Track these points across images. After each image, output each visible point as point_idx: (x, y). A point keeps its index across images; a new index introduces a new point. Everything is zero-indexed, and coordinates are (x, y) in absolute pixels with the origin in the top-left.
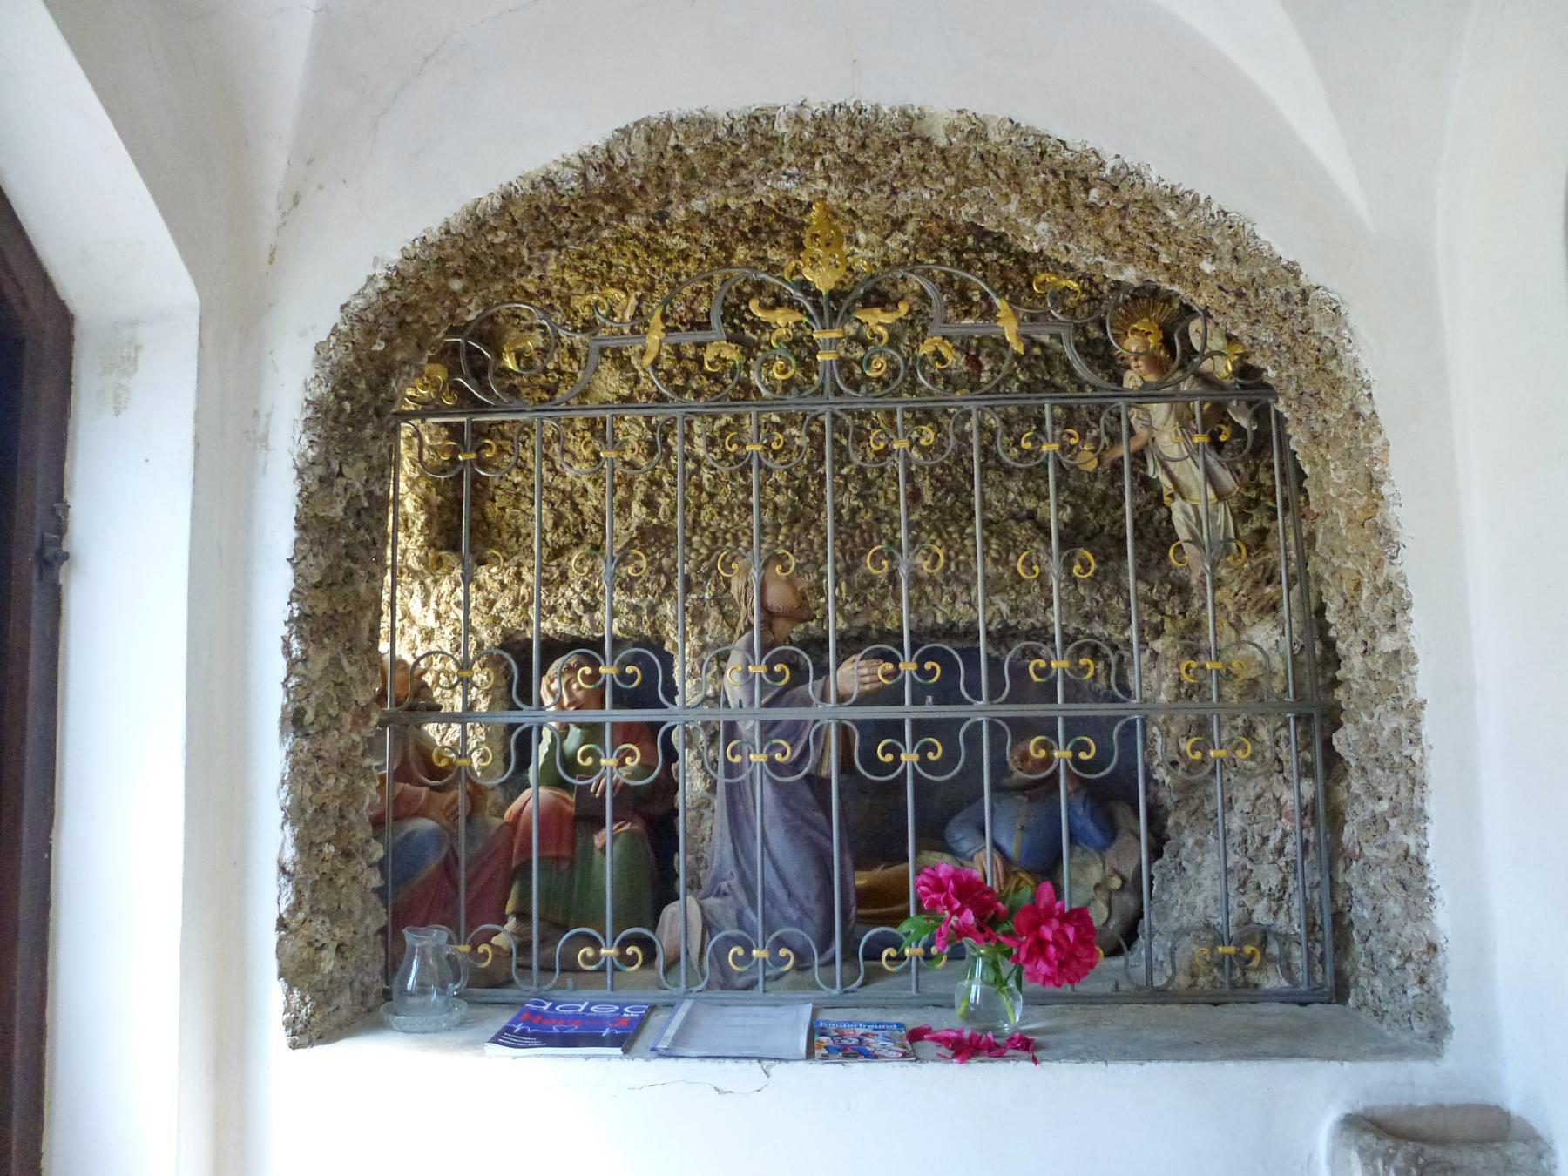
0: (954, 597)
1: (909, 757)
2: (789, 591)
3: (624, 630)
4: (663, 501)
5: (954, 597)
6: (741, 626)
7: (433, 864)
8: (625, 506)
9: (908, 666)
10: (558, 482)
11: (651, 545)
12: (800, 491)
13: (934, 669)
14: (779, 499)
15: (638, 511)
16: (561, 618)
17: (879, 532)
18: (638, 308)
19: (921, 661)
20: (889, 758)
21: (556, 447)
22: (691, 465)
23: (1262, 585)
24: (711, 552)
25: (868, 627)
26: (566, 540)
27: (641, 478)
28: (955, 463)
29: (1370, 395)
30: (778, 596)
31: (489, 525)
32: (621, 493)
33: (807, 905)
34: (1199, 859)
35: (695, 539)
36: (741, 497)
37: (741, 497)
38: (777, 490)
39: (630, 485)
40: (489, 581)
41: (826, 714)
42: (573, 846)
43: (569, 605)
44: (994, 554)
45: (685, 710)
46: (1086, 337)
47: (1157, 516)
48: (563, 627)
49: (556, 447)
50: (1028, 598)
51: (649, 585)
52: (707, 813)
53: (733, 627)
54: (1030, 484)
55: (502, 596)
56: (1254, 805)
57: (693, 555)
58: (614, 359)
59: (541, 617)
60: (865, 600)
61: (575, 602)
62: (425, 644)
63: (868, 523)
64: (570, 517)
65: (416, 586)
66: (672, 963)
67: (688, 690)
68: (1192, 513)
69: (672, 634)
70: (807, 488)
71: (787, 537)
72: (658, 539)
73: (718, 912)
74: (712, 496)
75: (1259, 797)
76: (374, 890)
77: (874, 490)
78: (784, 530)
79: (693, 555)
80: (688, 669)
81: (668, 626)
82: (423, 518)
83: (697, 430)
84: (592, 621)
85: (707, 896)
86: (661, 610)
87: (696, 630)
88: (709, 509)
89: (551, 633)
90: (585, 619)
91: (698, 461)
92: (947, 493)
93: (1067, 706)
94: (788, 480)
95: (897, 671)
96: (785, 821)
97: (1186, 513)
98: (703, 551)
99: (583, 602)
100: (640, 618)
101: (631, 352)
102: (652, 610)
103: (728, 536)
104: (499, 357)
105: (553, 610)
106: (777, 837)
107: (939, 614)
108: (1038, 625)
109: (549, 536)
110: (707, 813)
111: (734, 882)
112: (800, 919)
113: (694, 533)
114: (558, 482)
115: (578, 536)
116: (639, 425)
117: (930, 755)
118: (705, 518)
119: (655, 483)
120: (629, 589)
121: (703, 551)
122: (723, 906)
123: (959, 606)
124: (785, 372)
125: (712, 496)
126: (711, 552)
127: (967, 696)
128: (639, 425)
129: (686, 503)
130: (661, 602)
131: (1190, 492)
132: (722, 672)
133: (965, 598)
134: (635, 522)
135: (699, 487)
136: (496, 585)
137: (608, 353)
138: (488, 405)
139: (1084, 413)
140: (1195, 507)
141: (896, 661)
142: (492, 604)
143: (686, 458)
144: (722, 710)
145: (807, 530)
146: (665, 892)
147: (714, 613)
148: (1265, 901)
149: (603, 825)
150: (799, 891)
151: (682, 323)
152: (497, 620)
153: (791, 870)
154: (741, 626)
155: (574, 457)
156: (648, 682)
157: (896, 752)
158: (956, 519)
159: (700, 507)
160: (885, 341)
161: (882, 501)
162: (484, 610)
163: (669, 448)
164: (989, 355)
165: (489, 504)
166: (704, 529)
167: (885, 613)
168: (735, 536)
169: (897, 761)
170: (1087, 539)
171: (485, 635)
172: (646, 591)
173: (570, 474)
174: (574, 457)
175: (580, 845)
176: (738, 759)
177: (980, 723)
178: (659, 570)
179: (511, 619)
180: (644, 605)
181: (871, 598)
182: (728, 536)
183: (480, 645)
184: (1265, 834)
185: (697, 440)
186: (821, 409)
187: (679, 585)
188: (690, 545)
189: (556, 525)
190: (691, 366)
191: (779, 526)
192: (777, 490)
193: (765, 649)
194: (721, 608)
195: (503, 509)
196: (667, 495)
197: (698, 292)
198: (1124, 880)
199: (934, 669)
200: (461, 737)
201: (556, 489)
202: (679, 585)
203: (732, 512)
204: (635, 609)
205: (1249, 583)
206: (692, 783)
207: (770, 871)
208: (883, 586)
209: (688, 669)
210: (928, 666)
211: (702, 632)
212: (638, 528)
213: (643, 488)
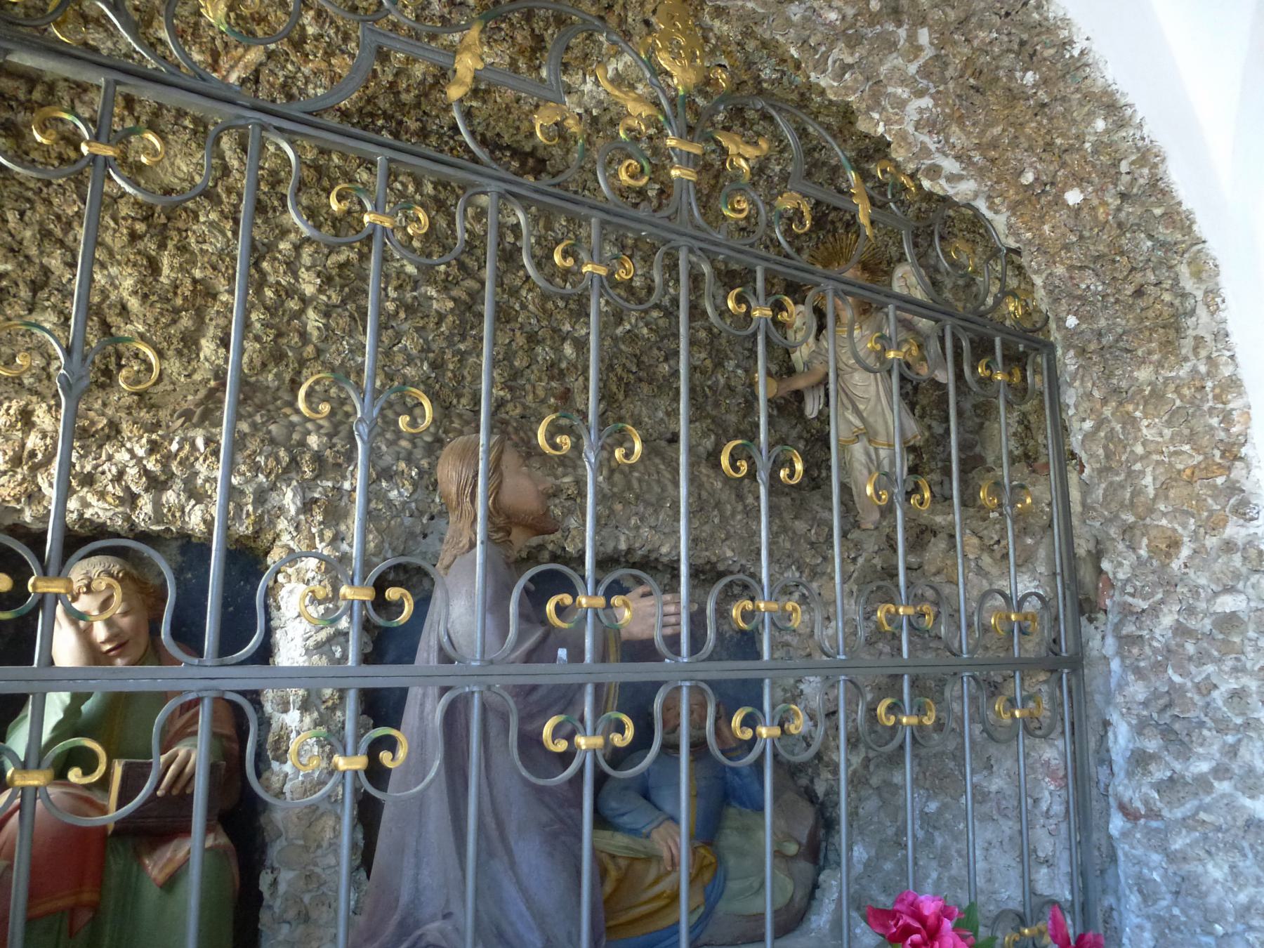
16: (102, 495)
18: (257, 72)
29: (1232, 357)
32: (186, 321)
43: (121, 474)
51: (261, 459)
58: (195, 132)
59: (66, 492)
68: (874, 457)
81: (282, 524)
83: (306, 260)
84: (157, 505)
86: (274, 498)
87: (328, 534)
93: (600, 667)
99: (146, 472)
100: (239, 507)
102: (261, 497)
105: (88, 480)
107: (623, 538)
116: (223, 233)
124: (632, 177)
128: (223, 233)
130: (273, 487)
135: (304, 335)
139: (724, 341)
149: (186, 831)
155: (111, 254)
161: (530, 397)
172: (257, 468)
174: (111, 254)
177: (473, 693)
180: (249, 490)
185: (303, 273)
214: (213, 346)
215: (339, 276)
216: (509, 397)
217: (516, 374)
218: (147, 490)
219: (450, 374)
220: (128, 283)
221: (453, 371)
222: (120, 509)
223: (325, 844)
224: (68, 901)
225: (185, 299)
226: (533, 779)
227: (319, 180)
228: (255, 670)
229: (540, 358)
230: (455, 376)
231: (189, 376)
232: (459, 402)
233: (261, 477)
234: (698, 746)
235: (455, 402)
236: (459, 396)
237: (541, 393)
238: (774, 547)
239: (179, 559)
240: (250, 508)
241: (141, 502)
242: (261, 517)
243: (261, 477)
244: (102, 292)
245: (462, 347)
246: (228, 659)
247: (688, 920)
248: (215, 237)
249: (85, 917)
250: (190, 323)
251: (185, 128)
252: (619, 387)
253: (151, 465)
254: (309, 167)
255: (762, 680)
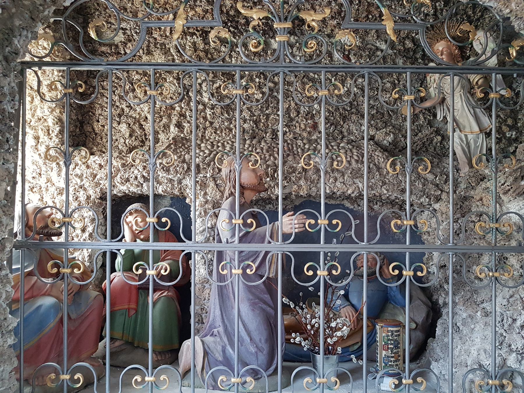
0: (336, 180)
1: (322, 273)
2: (253, 175)
3: (165, 191)
4: (186, 125)
5: (336, 180)
6: (227, 193)
7: (52, 323)
8: (166, 127)
9: (323, 222)
10: (132, 113)
11: (180, 147)
12: (256, 122)
13: (337, 223)
14: (246, 126)
15: (173, 130)
17: (296, 144)
19: (330, 219)
20: (311, 273)
21: (131, 94)
22: (201, 107)
23: (519, 180)
24: (211, 152)
25: (290, 194)
26: (136, 143)
27: (175, 113)
28: (335, 110)
30: (248, 178)
31: (96, 134)
32: (165, 120)
33: (260, 345)
34: (473, 326)
35: (203, 145)
36: (226, 124)
37: (226, 124)
38: (245, 121)
39: (169, 116)
40: (93, 164)
41: (278, 248)
42: (137, 303)
43: (136, 178)
44: (356, 158)
45: (197, 245)
46: (404, 47)
47: (435, 140)
48: (133, 189)
49: (131, 94)
50: (373, 181)
52: (207, 286)
53: (222, 192)
54: (372, 122)
55: (93, 173)
56: (508, 301)
57: (201, 154)
58: (161, 49)
60: (290, 179)
61: (139, 176)
62: (59, 196)
63: (291, 140)
64: (138, 132)
65: (54, 165)
66: (187, 372)
67: (198, 225)
68: (464, 139)
69: (190, 193)
70: (260, 121)
71: (250, 146)
72: (183, 145)
73: (212, 346)
74: (211, 123)
75: (511, 297)
76: (10, 346)
77: (294, 123)
78: (248, 142)
79: (201, 154)
80: (197, 213)
81: (188, 191)
82: (58, 129)
83: (205, 88)
85: (206, 336)
86: (184, 182)
87: (202, 193)
88: (210, 129)
89: (127, 192)
90: (145, 185)
91: (204, 105)
92: (331, 125)
94: (251, 116)
95: (317, 224)
96: (249, 300)
97: (461, 139)
98: (207, 152)
99: (143, 176)
101: (170, 45)
102: (180, 182)
103: (220, 144)
104: (85, 27)
105: (128, 180)
106: (245, 309)
108: (377, 194)
109: (127, 141)
110: (207, 286)
111: (221, 329)
112: (256, 352)
113: (202, 142)
114: (132, 113)
115: (142, 141)
116: (174, 85)
117: (334, 272)
118: (208, 134)
119: (182, 115)
120: (168, 171)
121: (207, 152)
122: (215, 342)
123: (338, 184)
124: (256, 47)
125: (211, 123)
126: (211, 152)
127: (356, 240)
129: (197, 127)
130: (184, 178)
131: (464, 127)
132: (216, 216)
133: (341, 180)
134: (172, 136)
135: (205, 118)
136: (97, 166)
137: (158, 46)
138: (79, 60)
140: (466, 136)
141: (316, 219)
142: (95, 176)
143: (198, 103)
144: (216, 244)
145: (260, 142)
146: (185, 334)
147: (212, 184)
148: (514, 355)
150: (256, 337)
151: (198, 31)
152: (98, 184)
153: (256, 337)
154: (227, 193)
156: (177, 227)
157: (315, 270)
158: (335, 139)
159: (205, 129)
160: (316, 31)
162: (91, 179)
163: (190, 97)
164: (355, 55)
165: (95, 123)
166: (207, 140)
167: (300, 187)
168: (223, 144)
169: (315, 275)
170: (400, 151)
171: (91, 192)
172: (177, 172)
173: (138, 110)
175: (141, 302)
176: (225, 272)
178: (184, 161)
179: (105, 184)
181: (294, 179)
182: (220, 144)
183: (89, 197)
184: (515, 317)
185: (204, 94)
186: (277, 70)
187: (193, 168)
188: (200, 148)
189: (131, 136)
190: (202, 54)
191: (245, 140)
192: (245, 121)
193: (243, 207)
194: (216, 181)
195: (103, 126)
196: (189, 122)
197: (206, 11)
198: (417, 325)
199: (337, 223)
200: (82, 242)
201: (131, 117)
202: (193, 168)
203: (221, 132)
204: (171, 181)
205: (511, 179)
206: (199, 271)
207: (241, 326)
208: (299, 173)
209: (197, 213)
210: (334, 222)
211: (206, 194)
212: (173, 139)
213: (176, 118)
214: (173, 128)
215: (216, 92)
216: (287, 130)
217: (292, 120)
218: (144, 182)
219: (262, 124)
220: (146, 109)
221: (263, 123)
222: (139, 188)
223: (207, 298)
224: (127, 307)
225: (164, 112)
226: (247, 283)
227: (207, 56)
228: (120, 243)
229: (302, 112)
230: (264, 125)
231: (168, 139)
232: (266, 135)
233: (178, 175)
234: (371, 275)
235: (264, 136)
236: (266, 133)
237: (303, 126)
238: (413, 187)
239: (171, 202)
240: (176, 185)
241: (144, 186)
242: (181, 189)
243: (178, 175)
244: (139, 114)
245: (267, 112)
246: (113, 240)
247: (409, 348)
248: (172, 87)
249: (132, 312)
250: (166, 120)
251: (158, 48)
252: (340, 118)
253: (146, 175)
254: (202, 51)
255: (320, 252)
